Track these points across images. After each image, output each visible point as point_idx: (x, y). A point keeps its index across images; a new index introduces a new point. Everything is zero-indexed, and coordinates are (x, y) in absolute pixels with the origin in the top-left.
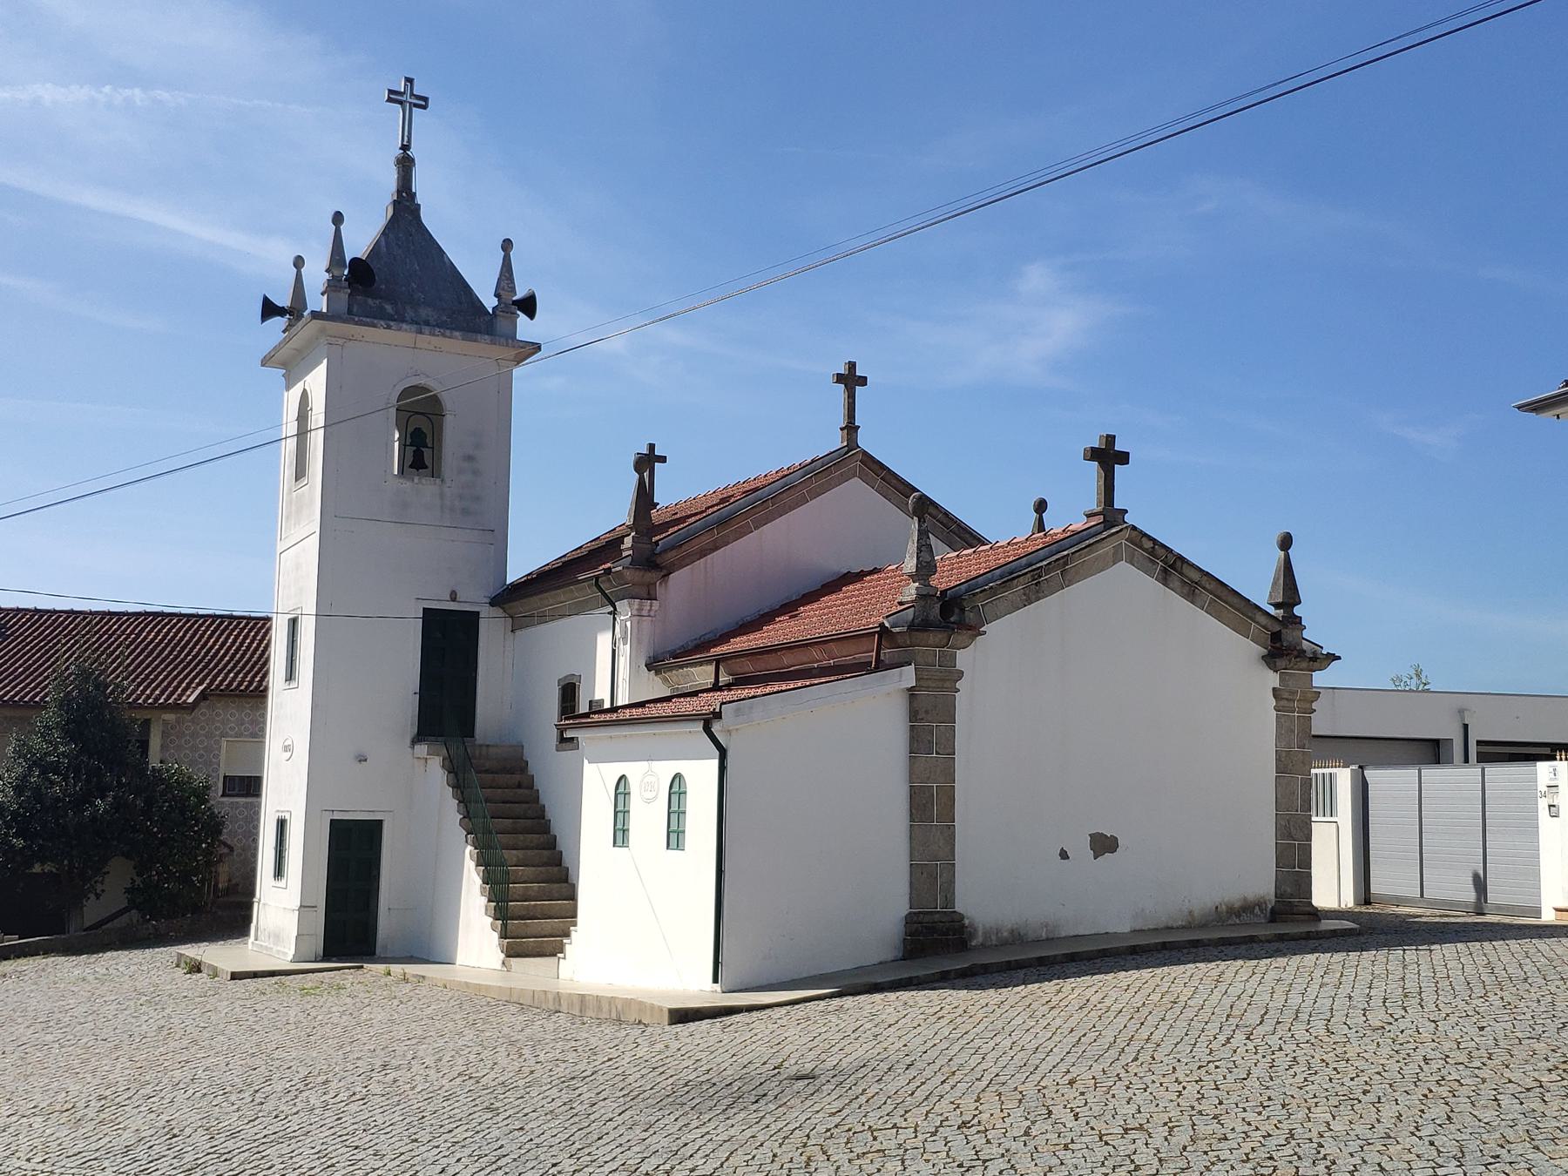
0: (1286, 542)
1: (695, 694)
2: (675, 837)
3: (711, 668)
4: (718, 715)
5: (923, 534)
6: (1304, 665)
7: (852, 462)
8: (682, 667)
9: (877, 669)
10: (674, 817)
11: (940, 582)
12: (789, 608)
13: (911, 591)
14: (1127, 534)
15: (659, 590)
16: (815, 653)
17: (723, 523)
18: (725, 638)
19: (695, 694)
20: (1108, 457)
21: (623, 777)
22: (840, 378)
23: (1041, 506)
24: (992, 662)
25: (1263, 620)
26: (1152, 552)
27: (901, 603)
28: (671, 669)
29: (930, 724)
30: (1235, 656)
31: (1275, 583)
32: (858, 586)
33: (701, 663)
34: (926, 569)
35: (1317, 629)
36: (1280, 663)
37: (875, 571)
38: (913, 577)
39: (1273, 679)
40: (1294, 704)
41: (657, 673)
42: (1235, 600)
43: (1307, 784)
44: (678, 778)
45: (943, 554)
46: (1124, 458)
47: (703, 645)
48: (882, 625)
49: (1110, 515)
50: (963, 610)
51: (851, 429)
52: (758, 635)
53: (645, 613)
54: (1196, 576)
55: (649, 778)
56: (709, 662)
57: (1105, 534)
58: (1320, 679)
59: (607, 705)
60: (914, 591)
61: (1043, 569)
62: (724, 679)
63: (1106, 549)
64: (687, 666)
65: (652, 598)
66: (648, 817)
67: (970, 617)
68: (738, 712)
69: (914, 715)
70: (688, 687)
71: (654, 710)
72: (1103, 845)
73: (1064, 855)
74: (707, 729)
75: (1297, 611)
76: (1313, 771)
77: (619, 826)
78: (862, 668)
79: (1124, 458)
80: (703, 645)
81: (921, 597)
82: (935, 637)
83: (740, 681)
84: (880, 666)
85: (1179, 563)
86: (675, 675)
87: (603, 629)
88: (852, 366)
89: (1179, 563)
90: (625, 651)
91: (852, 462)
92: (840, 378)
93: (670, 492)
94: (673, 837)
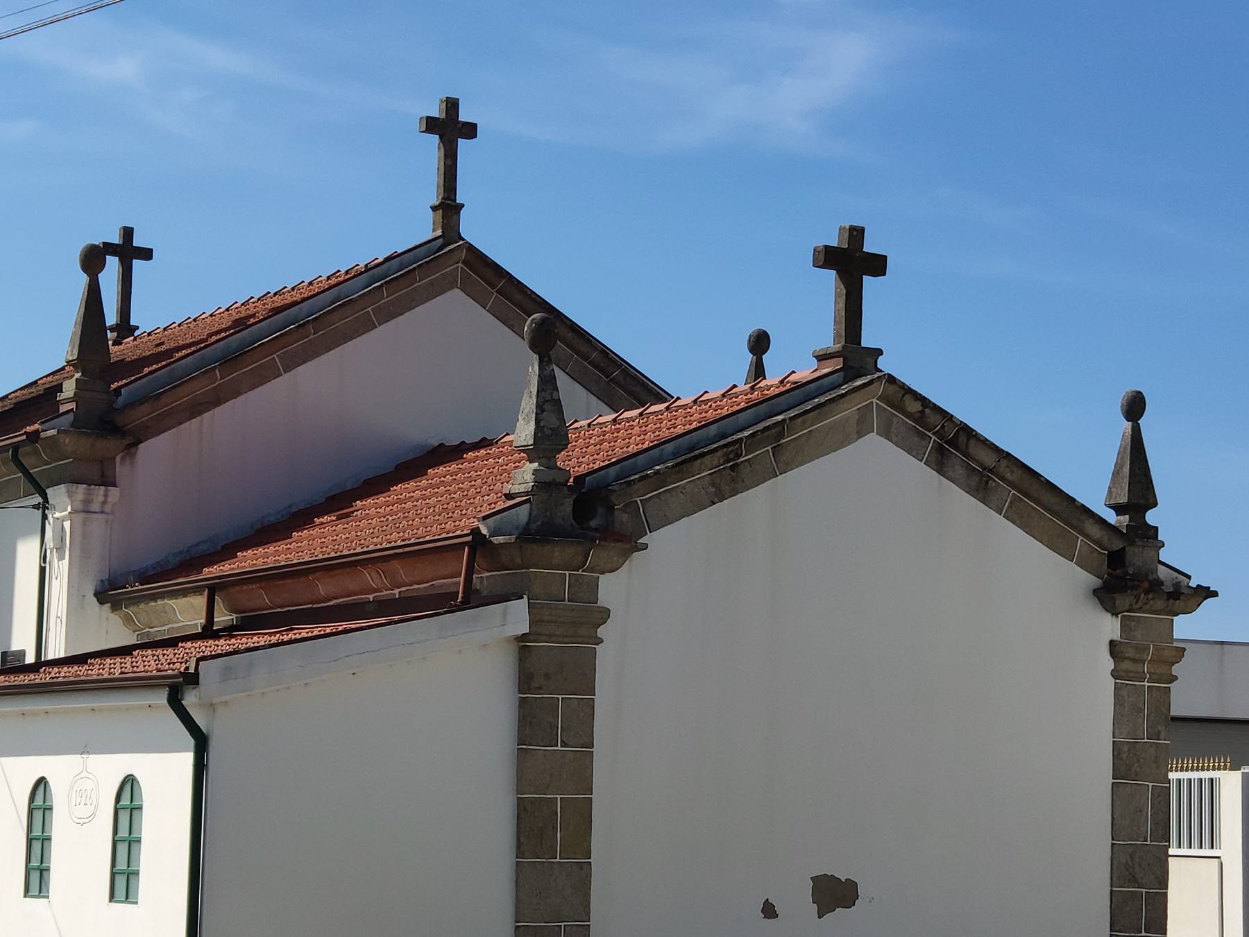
0: (1135, 407)
1: (172, 643)
2: (123, 882)
3: (200, 601)
4: (192, 679)
5: (547, 383)
6: (1160, 604)
7: (450, 263)
8: (154, 598)
9: (467, 604)
10: (122, 849)
11: (577, 460)
12: (339, 502)
13: (525, 475)
14: (880, 388)
15: (121, 470)
16: (369, 577)
17: (231, 360)
18: (228, 551)
19: (172, 643)
20: (852, 262)
21: (42, 781)
22: (431, 125)
23: (760, 343)
24: (656, 593)
25: (1095, 531)
26: (920, 419)
27: (509, 496)
28: (136, 600)
29: (552, 700)
30: (1047, 588)
31: (1116, 473)
32: (453, 467)
33: (184, 593)
34: (551, 438)
35: (1182, 545)
36: (1123, 600)
37: (484, 443)
38: (532, 453)
39: (1110, 627)
40: (1143, 666)
41: (116, 607)
42: (1047, 498)
43: (1163, 795)
44: (129, 783)
45: (588, 417)
46: (877, 265)
47: (190, 562)
48: (475, 532)
49: (853, 357)
50: (610, 509)
51: (449, 208)
52: (282, 546)
53: (96, 507)
54: (989, 459)
55: (82, 783)
56: (197, 591)
57: (844, 389)
58: (1185, 627)
59: (30, 659)
60: (529, 477)
61: (747, 442)
62: (223, 618)
63: (847, 412)
64: (162, 596)
65: (107, 481)
66: (81, 848)
67: (623, 519)
68: (227, 673)
69: (525, 681)
70: (162, 631)
71: (95, 670)
72: (834, 894)
73: (769, 911)
74: (176, 703)
75: (1151, 517)
76: (1172, 776)
77: (35, 863)
78: (440, 603)
79: (877, 265)
80: (190, 562)
81: (542, 485)
82: (561, 552)
83: (249, 622)
84: (472, 599)
85: (962, 439)
86: (143, 611)
87: (26, 534)
88: (452, 105)
89: (962, 439)
90: (60, 570)
91: (450, 263)
92: (431, 125)
93: (166, 302)
94: (121, 882)
